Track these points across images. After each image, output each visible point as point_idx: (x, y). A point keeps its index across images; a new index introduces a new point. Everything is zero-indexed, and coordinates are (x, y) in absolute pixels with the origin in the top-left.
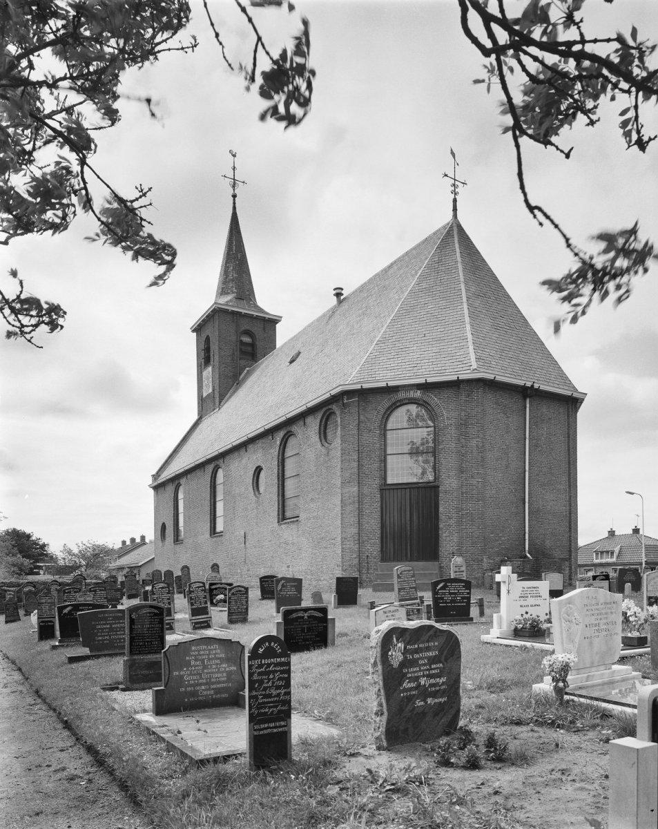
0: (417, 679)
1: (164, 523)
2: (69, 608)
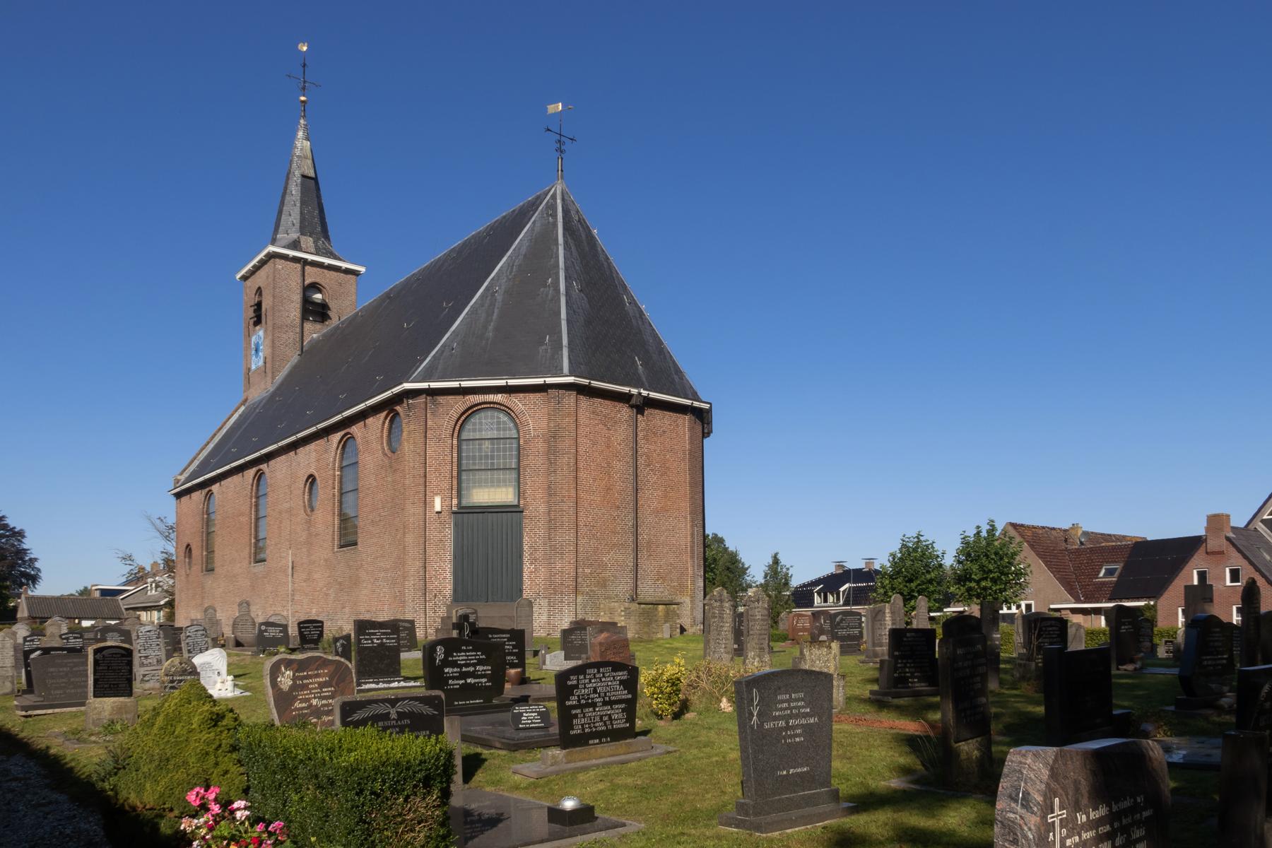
0: (308, 700)
1: (188, 545)
2: (38, 653)
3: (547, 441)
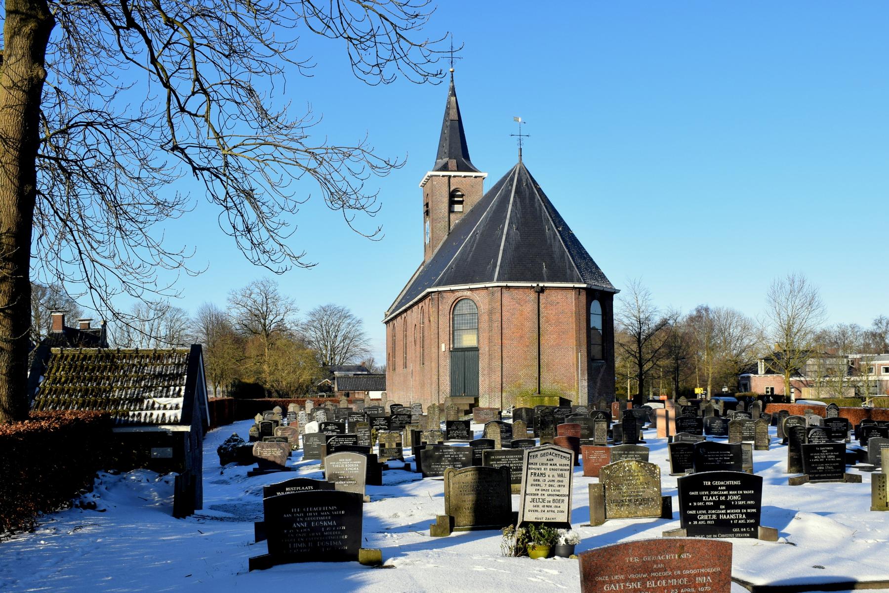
3: (488, 315)
